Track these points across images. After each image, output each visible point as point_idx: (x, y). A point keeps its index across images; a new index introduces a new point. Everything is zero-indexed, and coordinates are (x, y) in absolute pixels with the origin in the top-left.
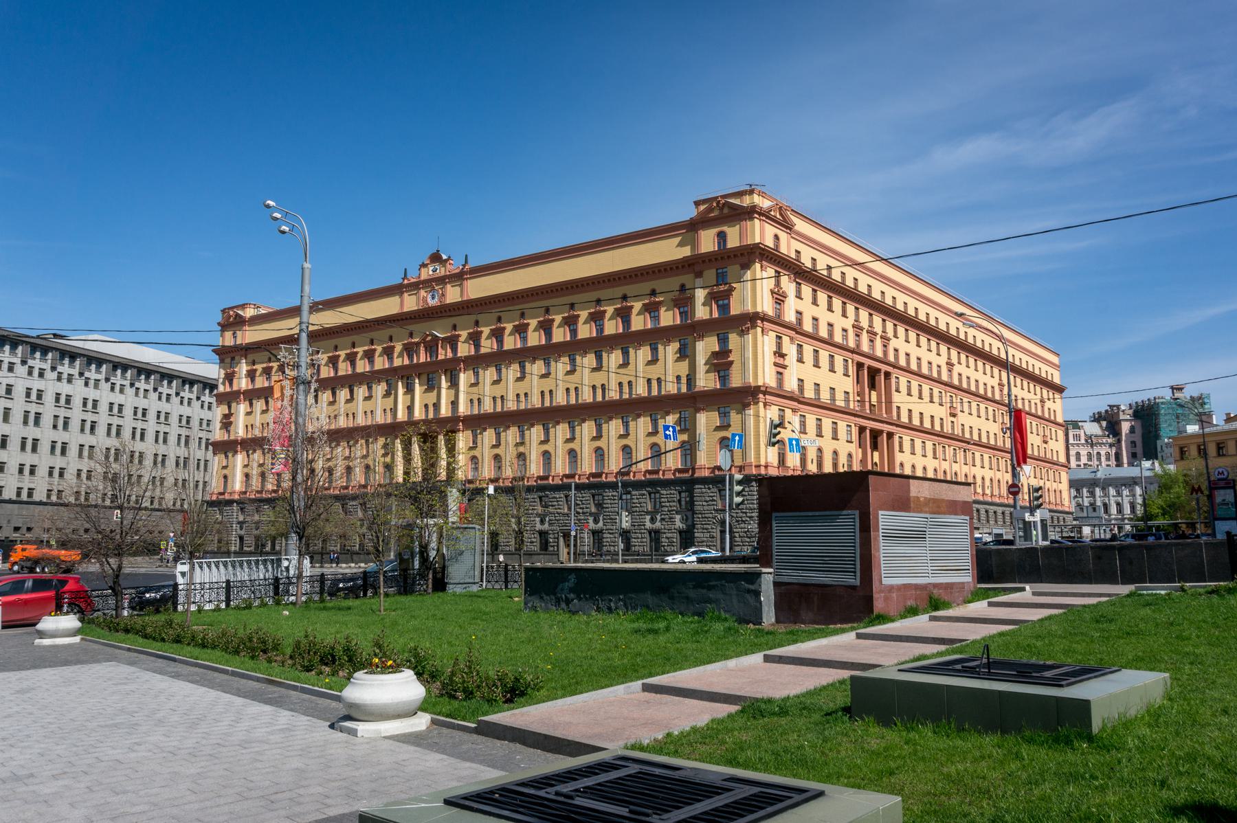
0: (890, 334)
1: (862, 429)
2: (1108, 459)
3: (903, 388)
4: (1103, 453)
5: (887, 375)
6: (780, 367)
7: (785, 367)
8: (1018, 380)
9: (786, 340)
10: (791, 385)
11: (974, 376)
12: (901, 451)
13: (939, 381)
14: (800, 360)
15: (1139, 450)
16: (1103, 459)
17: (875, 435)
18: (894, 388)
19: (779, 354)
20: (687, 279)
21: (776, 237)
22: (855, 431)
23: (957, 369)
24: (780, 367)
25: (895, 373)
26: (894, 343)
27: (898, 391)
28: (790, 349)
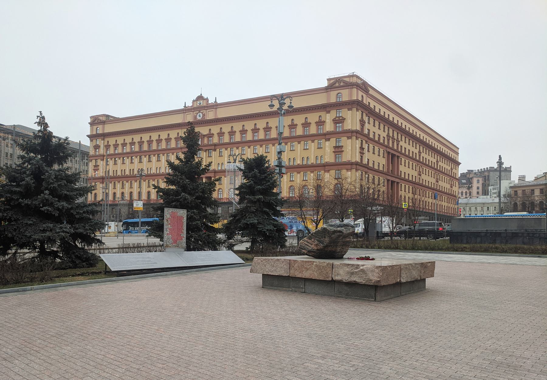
0: (422, 151)
1: (388, 180)
2: (466, 194)
3: (403, 163)
4: (464, 191)
5: (398, 157)
6: (362, 153)
7: (363, 154)
8: (403, 137)
9: (364, 142)
10: (365, 161)
14: (368, 151)
15: (480, 190)
16: (464, 194)
17: (393, 182)
19: (362, 148)
20: (323, 114)
21: (362, 96)
23: (422, 155)
24: (362, 153)
27: (401, 164)
28: (365, 146)
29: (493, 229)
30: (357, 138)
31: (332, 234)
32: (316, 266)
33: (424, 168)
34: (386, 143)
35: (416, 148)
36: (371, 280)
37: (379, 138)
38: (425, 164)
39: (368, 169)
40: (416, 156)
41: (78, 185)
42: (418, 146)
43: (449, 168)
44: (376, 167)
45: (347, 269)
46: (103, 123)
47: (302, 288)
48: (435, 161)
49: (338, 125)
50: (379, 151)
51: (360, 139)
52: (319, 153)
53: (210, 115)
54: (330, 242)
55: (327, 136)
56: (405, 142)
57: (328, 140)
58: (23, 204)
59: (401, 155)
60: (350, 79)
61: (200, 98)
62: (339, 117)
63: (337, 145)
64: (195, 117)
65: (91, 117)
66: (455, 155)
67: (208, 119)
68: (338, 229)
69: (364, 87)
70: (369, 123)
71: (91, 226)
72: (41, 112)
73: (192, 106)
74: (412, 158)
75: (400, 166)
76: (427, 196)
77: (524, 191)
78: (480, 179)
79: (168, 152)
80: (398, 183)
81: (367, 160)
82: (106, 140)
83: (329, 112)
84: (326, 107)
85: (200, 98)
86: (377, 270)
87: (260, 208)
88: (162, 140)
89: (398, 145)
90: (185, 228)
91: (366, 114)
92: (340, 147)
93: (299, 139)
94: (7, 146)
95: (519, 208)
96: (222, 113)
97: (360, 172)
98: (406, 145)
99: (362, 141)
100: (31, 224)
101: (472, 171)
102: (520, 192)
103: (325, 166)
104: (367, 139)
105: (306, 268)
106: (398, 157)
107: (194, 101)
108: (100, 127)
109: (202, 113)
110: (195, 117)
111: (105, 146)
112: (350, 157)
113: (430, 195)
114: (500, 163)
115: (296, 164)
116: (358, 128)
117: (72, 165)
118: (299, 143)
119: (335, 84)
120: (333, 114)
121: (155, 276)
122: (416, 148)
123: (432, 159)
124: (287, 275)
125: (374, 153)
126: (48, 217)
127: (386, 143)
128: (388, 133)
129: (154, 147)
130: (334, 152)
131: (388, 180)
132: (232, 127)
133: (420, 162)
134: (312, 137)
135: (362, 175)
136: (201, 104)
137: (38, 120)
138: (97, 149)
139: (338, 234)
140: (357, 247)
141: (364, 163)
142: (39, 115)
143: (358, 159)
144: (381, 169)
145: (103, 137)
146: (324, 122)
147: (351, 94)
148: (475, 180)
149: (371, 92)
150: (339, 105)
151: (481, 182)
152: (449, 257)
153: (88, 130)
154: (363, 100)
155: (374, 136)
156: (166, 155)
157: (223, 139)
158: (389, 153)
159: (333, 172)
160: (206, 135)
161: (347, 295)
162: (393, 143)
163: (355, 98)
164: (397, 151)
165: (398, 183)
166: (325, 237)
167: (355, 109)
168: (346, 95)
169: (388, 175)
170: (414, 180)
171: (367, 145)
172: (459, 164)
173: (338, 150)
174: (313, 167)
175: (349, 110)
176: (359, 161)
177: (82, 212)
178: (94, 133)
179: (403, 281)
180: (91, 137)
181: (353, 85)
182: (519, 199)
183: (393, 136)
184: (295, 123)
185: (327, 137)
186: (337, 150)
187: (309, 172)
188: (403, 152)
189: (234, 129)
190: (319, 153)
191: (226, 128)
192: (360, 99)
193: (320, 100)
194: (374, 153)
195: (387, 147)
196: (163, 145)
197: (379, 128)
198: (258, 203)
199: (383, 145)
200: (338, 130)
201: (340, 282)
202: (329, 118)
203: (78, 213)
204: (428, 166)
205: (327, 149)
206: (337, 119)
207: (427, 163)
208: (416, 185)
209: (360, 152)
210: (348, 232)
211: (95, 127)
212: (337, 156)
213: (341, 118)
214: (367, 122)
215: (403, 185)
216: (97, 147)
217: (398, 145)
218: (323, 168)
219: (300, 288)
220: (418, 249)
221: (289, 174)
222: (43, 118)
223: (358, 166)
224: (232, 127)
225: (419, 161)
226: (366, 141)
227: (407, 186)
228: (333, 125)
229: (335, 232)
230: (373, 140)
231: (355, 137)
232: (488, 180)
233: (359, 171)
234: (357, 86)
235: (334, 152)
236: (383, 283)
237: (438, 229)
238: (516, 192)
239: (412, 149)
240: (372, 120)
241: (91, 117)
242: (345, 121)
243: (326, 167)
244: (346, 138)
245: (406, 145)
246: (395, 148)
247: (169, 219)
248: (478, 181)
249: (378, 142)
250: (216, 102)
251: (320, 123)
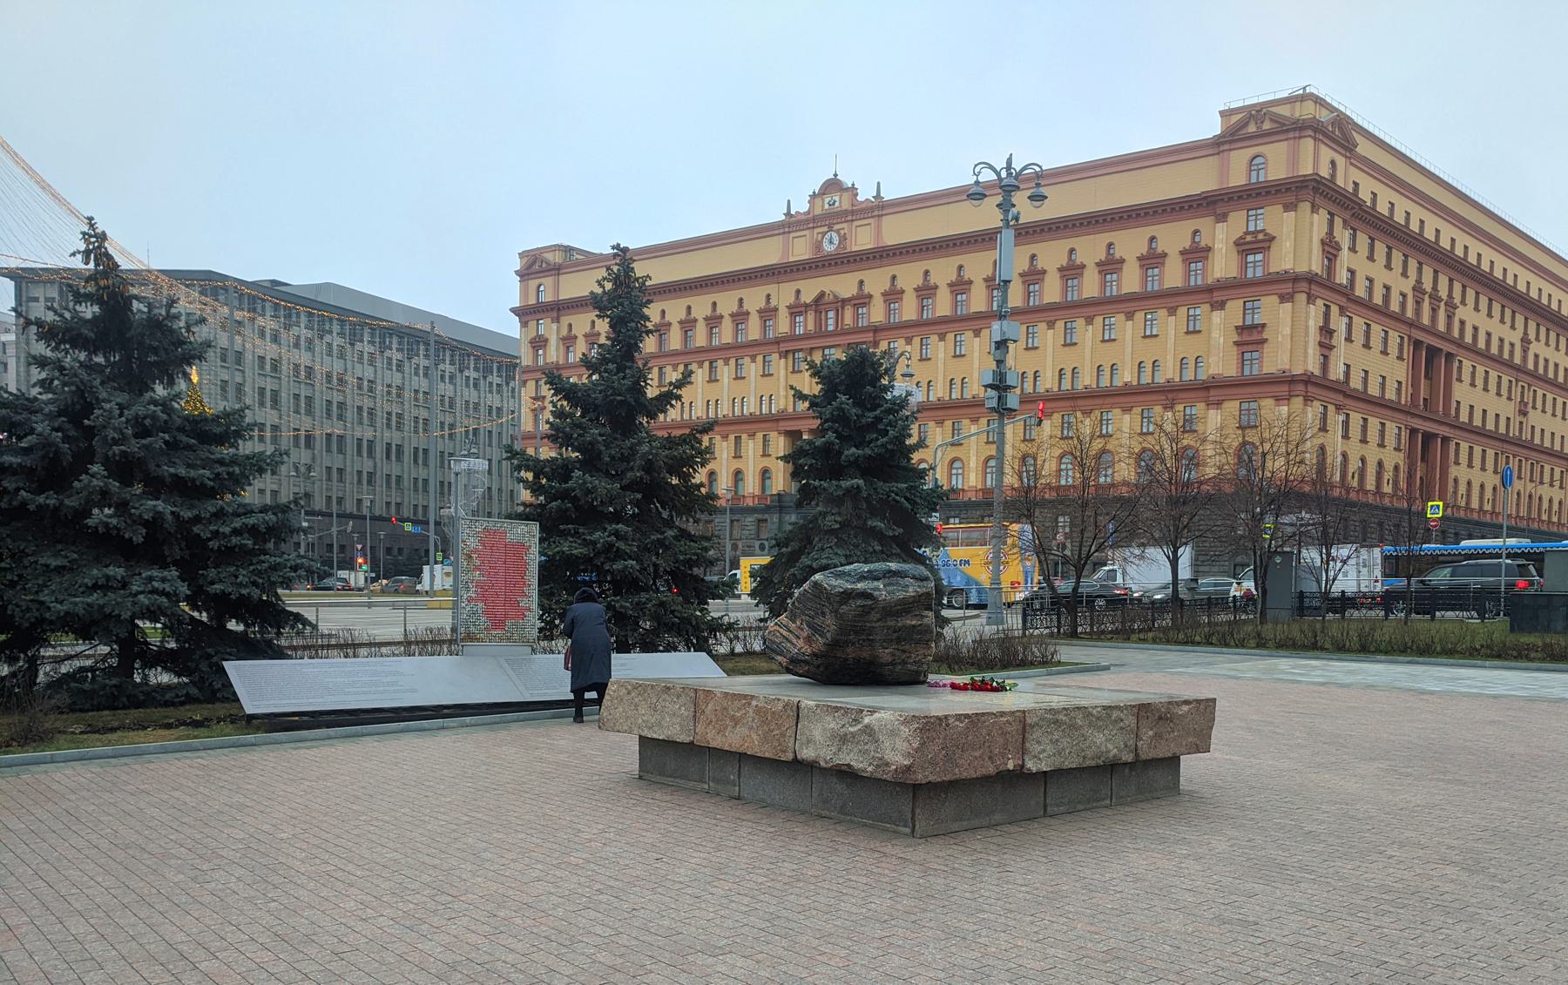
0: (1532, 336)
1: (1413, 432)
3: (1466, 377)
6: (1326, 347)
7: (1331, 348)
8: (1470, 294)
9: (1335, 309)
10: (1337, 372)
11: (1485, 324)
12: (1457, 463)
13: (1509, 365)
14: (1349, 339)
17: (1428, 438)
18: (1455, 376)
19: (1326, 330)
20: (1204, 223)
21: (1333, 163)
22: (1405, 435)
23: (1535, 348)
24: (1326, 347)
25: (1461, 355)
26: (1461, 313)
27: (1460, 380)
28: (1339, 324)
30: (1311, 299)
31: (841, 603)
33: (1540, 393)
34: (1410, 314)
35: (1513, 327)
36: (887, 764)
37: (1386, 298)
38: (1544, 379)
39: (1346, 395)
40: (1512, 353)
41: (246, 448)
42: (1520, 319)
44: (1374, 390)
45: (832, 724)
46: (556, 270)
49: (1250, 258)
50: (1385, 340)
51: (1320, 302)
52: (1192, 347)
53: (863, 238)
54: (842, 630)
55: (1215, 294)
57: (1221, 305)
58: (32, 507)
60: (1293, 109)
61: (833, 185)
62: (1257, 232)
63: (1249, 322)
64: (818, 246)
65: (522, 255)
67: (854, 249)
68: (859, 586)
69: (1339, 132)
70: (1353, 249)
71: (259, 573)
72: (90, 219)
73: (808, 213)
74: (1497, 360)
75: (1456, 385)
76: (1547, 478)
79: (738, 353)
80: (1445, 440)
81: (1342, 368)
82: (565, 320)
83: (1222, 218)
84: (1215, 202)
85: (833, 185)
86: (905, 731)
87: (859, 517)
88: (722, 317)
89: (1450, 318)
91: (1345, 221)
93: (1130, 306)
94: (297, 345)
96: (897, 232)
97: (1317, 407)
98: (1479, 319)
99: (1327, 307)
100: (64, 567)
103: (1207, 388)
104: (1343, 301)
105: (733, 718)
107: (814, 196)
108: (548, 282)
109: (838, 231)
110: (818, 246)
111: (564, 339)
112: (1286, 360)
113: (1557, 476)
115: (1118, 383)
116: (1316, 265)
117: (201, 388)
118: (1130, 316)
119: (1248, 127)
120: (1237, 223)
121: (402, 731)
122: (1513, 327)
124: (687, 740)
125: (1367, 346)
126: (109, 544)
128: (1419, 282)
129: (700, 338)
130: (1237, 344)
131: (1413, 432)
132: (927, 273)
134: (1170, 299)
135: (1325, 415)
136: (836, 205)
137: (82, 247)
138: (540, 347)
139: (859, 602)
140: (1193, 643)
141: (1332, 377)
142: (86, 229)
143: (1313, 366)
144: (1391, 395)
145: (555, 314)
146: (1208, 249)
147: (1294, 159)
150: (1255, 195)
152: (1440, 679)
153: (513, 294)
154: (1333, 175)
155: (1370, 290)
156: (732, 361)
157: (900, 309)
158: (1417, 344)
159: (1232, 407)
160: (849, 300)
161: (842, 810)
162: (1434, 310)
163: (1307, 169)
165: (1445, 440)
167: (1306, 206)
168: (1277, 162)
169: (1414, 415)
170: (1502, 430)
171: (1345, 320)
173: (1250, 337)
174: (1170, 393)
176: (1317, 372)
177: (227, 530)
178: (532, 301)
179: (1031, 765)
180: (525, 313)
181: (1301, 129)
183: (1435, 288)
184: (1117, 256)
185: (1218, 296)
186: (1246, 338)
187: (1117, 411)
188: (1468, 339)
189: (933, 280)
190: (1192, 347)
191: (909, 275)
192: (1325, 172)
193: (1198, 179)
194: (1367, 346)
196: (726, 334)
197: (1388, 267)
198: (849, 504)
199: (1398, 318)
200: (1250, 275)
201: (810, 767)
202: (1222, 236)
203: (216, 534)
205: (1215, 334)
206: (1249, 238)
207: (1551, 375)
208: (1514, 446)
209: (1321, 344)
210: (901, 595)
211: (533, 284)
212: (1247, 356)
213: (1261, 237)
214: (1345, 245)
215: (1464, 446)
216: (539, 343)
217: (1450, 318)
218: (1202, 394)
220: (1378, 651)
221: (1097, 413)
222: (103, 237)
223: (1310, 388)
224: (927, 273)
225: (1520, 370)
226: (1341, 308)
227: (1478, 450)
228: (1234, 257)
229: (847, 596)
230: (1366, 305)
231: (1303, 297)
233: (1317, 404)
234: (1315, 130)
235: (1237, 344)
236: (920, 777)
237: (1510, 585)
239: (1499, 330)
240: (1363, 240)
241: (522, 255)
242: (1274, 246)
243: (1211, 390)
244: (1275, 299)
245: (1479, 319)
246: (1441, 327)
247: (476, 551)
249: (1382, 312)
250: (878, 196)
251: (1196, 253)
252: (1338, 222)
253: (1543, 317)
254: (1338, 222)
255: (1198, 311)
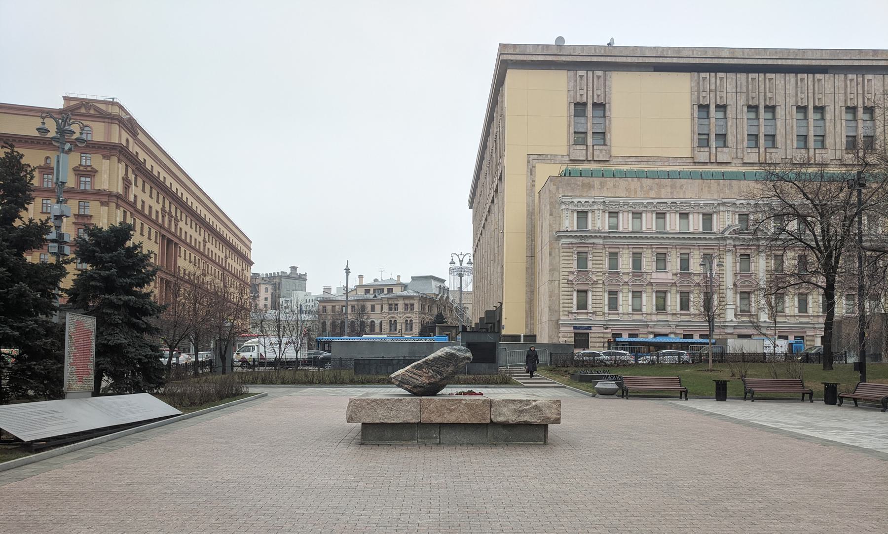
8: (184, 216)
9: (128, 214)
15: (269, 303)
21: (127, 140)
29: (377, 355)
30: (118, 207)
32: (467, 405)
38: (211, 260)
43: (240, 269)
47: (436, 438)
48: (223, 256)
49: (83, 179)
56: (186, 224)
59: (180, 243)
62: (86, 166)
63: (82, 213)
66: (248, 251)
69: (131, 126)
77: (334, 307)
78: (269, 287)
89: (176, 226)
90: (93, 353)
92: (87, 216)
95: (377, 329)
98: (187, 229)
101: (259, 275)
102: (329, 308)
104: (132, 210)
105: (449, 409)
106: (176, 244)
114: (294, 269)
119: (79, 109)
123: (219, 253)
127: (160, 221)
128: (164, 206)
133: (205, 256)
148: (262, 288)
149: (141, 136)
151: (270, 291)
158: (163, 236)
164: (174, 235)
166: (448, 366)
172: (251, 263)
175: (105, 157)
181: (112, 119)
182: (329, 317)
183: (170, 211)
195: (161, 227)
201: (505, 425)
204: (214, 262)
206: (82, 168)
213: (89, 169)
217: (176, 226)
219: (431, 438)
225: (203, 254)
232: (279, 289)
234: (120, 122)
238: (325, 307)
242: (97, 174)
244: (98, 203)
246: (173, 230)
247: (73, 334)
248: (267, 289)
252: (130, 170)
253: (162, 190)
254: (130, 170)
255: (49, 202)
